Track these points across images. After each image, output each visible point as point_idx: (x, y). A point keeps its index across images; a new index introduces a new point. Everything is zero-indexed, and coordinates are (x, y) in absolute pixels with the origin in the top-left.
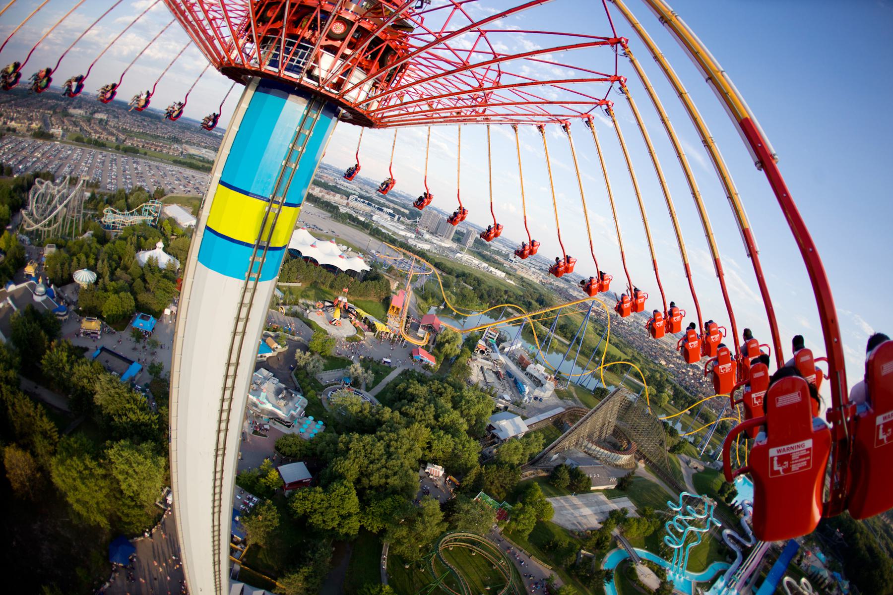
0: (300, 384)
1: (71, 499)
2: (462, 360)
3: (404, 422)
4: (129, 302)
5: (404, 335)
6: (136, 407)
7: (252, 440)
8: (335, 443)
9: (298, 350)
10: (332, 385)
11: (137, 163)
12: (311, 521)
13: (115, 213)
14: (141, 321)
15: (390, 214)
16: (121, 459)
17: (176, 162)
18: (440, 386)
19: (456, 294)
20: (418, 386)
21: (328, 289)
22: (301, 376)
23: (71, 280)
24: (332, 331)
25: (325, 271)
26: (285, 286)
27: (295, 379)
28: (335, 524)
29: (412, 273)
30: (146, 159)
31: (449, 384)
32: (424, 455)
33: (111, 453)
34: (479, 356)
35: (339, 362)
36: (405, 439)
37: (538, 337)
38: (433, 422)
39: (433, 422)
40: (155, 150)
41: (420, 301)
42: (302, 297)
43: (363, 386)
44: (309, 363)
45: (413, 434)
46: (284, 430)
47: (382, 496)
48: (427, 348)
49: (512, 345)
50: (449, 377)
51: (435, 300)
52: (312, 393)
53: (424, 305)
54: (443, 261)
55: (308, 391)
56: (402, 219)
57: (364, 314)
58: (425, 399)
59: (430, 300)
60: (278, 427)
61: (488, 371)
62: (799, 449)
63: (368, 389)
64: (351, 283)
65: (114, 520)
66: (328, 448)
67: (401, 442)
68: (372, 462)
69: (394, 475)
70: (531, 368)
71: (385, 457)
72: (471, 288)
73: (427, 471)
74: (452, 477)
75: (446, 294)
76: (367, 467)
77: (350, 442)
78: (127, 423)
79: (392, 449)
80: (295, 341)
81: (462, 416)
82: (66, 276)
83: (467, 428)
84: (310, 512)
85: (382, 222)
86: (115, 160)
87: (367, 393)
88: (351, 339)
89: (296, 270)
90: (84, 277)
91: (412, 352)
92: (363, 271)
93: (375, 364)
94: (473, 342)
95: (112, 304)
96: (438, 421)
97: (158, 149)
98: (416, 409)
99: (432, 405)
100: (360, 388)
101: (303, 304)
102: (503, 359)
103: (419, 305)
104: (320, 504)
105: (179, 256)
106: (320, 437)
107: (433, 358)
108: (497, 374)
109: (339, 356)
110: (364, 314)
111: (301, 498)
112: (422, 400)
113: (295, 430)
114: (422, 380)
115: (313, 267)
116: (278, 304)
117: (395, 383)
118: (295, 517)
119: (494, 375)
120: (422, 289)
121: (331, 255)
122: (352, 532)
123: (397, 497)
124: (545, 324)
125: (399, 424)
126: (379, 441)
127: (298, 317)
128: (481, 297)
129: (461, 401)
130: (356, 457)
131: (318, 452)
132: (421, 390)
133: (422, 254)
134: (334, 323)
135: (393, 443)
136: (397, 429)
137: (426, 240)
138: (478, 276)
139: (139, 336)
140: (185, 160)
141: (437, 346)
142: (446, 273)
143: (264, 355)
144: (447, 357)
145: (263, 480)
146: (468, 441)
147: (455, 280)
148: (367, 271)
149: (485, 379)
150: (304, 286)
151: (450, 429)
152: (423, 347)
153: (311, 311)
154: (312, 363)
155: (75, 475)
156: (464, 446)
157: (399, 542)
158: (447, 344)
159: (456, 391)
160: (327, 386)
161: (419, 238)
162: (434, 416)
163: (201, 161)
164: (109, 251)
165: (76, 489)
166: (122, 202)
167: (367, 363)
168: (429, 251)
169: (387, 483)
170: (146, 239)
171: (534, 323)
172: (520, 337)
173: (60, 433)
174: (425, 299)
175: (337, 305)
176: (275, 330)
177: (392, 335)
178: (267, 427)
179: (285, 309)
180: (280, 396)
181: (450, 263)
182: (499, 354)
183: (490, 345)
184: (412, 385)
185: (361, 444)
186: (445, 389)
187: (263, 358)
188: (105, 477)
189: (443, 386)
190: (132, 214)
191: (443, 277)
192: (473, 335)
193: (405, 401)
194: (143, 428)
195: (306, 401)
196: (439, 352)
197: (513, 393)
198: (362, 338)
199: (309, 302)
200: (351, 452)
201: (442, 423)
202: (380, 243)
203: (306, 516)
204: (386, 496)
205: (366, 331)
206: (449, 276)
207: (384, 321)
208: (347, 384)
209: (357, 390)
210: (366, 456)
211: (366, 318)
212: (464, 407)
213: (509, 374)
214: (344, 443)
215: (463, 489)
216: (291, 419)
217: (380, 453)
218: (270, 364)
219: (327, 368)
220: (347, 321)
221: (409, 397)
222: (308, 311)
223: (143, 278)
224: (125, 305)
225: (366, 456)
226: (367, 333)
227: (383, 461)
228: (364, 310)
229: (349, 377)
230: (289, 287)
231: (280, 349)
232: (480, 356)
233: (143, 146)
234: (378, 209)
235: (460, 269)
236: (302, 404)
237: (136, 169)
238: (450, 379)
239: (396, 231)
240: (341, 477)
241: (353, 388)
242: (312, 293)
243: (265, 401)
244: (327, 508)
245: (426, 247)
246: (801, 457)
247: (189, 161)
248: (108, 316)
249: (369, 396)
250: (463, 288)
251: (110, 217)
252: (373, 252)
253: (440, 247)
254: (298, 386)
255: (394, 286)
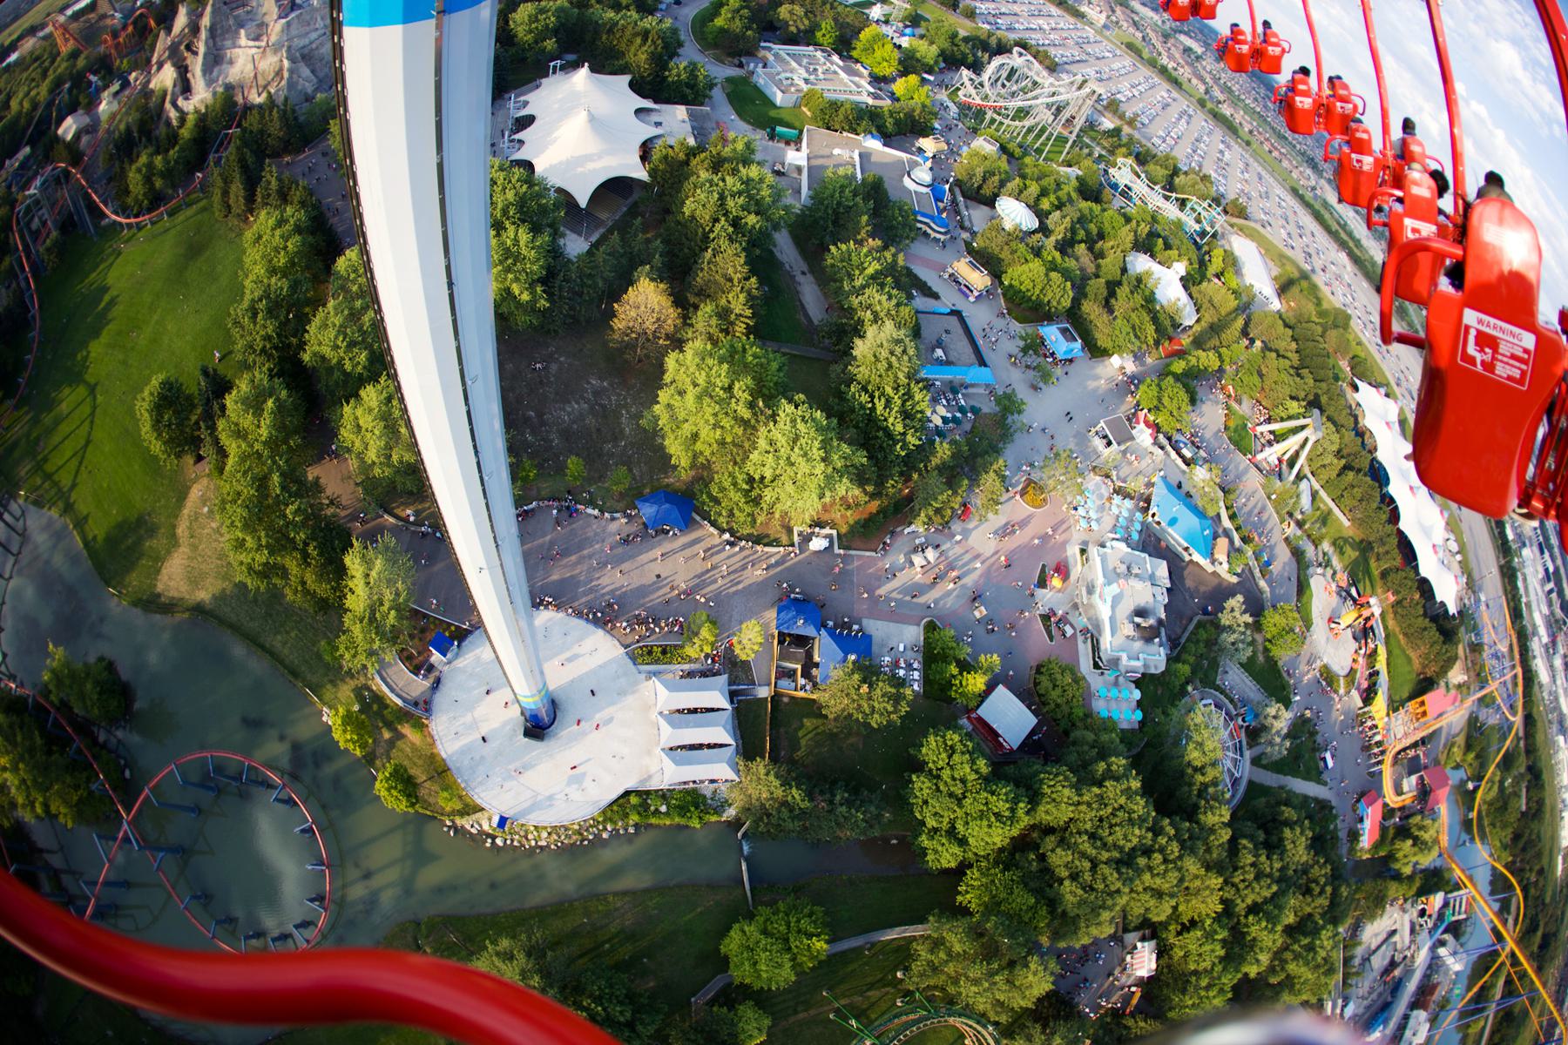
0: (1188, 640)
1: (663, 396)
2: (1394, 889)
3: (1215, 855)
4: (1059, 295)
5: (1388, 758)
6: (899, 402)
7: (1029, 621)
8: (1103, 755)
9: (1240, 598)
10: (1226, 696)
11: (1228, 147)
12: (914, 778)
13: (1139, 177)
14: (1058, 332)
15: (1546, 570)
16: (788, 427)
17: (1295, 192)
18: (1323, 881)
19: (1502, 788)
20: (1302, 842)
21: (1376, 573)
22: (1203, 635)
23: (990, 202)
24: (1319, 630)
25: (1394, 541)
26: (1326, 504)
27: (1191, 627)
28: (931, 823)
29: (1493, 686)
30: (1247, 151)
31: (1335, 893)
32: (1164, 925)
33: (786, 409)
34: (1413, 913)
35: (1274, 681)
36: (1176, 874)
37: (1482, 988)
38: (1241, 907)
39: (1241, 907)
40: (1270, 152)
41: (1461, 740)
42: (1334, 544)
43: (1257, 750)
44: (1234, 632)
45: (1198, 883)
46: (1085, 665)
47: (1032, 885)
48: (1388, 812)
49: (1454, 953)
50: (1349, 885)
51: (1476, 764)
52: (1184, 669)
53: (1457, 753)
54: (1539, 724)
55: (1184, 662)
56: (1554, 595)
57: (1381, 664)
58: (1281, 870)
59: (1471, 756)
60: (1084, 649)
61: (1391, 948)
62: (1511, 339)
63: (1256, 761)
64: (1412, 599)
65: (703, 473)
66: (1086, 748)
67: (1166, 871)
68: (1093, 836)
69: (1083, 889)
70: (1421, 1015)
71: (1116, 854)
72: (1524, 808)
73: (1139, 945)
74: (1138, 995)
75: (1494, 774)
76: (1079, 833)
77: (1117, 779)
78: (862, 407)
79: (1142, 861)
80: (1257, 585)
81: (1278, 955)
82: (987, 191)
83: (1252, 975)
84: (931, 770)
85: (1529, 570)
86: (1190, 116)
87: (1248, 763)
88: (1328, 676)
89: (1359, 496)
90: (1014, 213)
91: (1369, 790)
92: (1443, 604)
93: (1310, 744)
94: (1436, 884)
95: (1026, 274)
96: (1246, 917)
97: (1275, 154)
98: (1253, 865)
99: (1275, 888)
100: (1250, 746)
101: (1325, 554)
102: (1422, 957)
103: (1453, 744)
104: (954, 779)
105: (1202, 311)
106: (1108, 725)
107: (1377, 836)
108: (1393, 964)
109: (1285, 675)
110: (1381, 664)
111: (949, 743)
112: (1277, 865)
113: (1095, 681)
114: (1321, 843)
115: (1384, 517)
116: (1290, 515)
117: (1289, 799)
118: (912, 751)
119: (1386, 962)
120: (1480, 728)
121: (1426, 532)
122: (930, 857)
123: (1044, 911)
124: (1509, 982)
125: (1208, 850)
126: (1148, 829)
127: (1298, 562)
128: (1517, 837)
129: (1305, 935)
130: (1089, 804)
131: (1072, 735)
132: (1298, 848)
133: (1529, 677)
134: (1333, 625)
135: (1158, 857)
136: (1193, 851)
137: (1552, 666)
138: (1547, 802)
139: (1035, 346)
140: (1312, 202)
141: (1400, 826)
142: (1526, 745)
143: (1191, 550)
144: (1391, 857)
145: (954, 670)
146: (1222, 991)
147: (1522, 770)
148: (1446, 611)
149: (1375, 951)
150: (1351, 533)
151: (1238, 946)
152: (1385, 805)
153: (1324, 575)
154: (1235, 636)
155: (701, 380)
156: (1208, 988)
157: (937, 944)
158: (1410, 842)
159: (1323, 916)
160: (1217, 688)
161: (1547, 651)
162: (1255, 904)
163: (1339, 224)
164: (1087, 212)
165: (682, 393)
166: (1161, 173)
167: (1303, 730)
168: (1541, 686)
169: (1061, 881)
170: (1168, 247)
171: (1503, 964)
172: (1474, 957)
173: (749, 330)
174: (1468, 747)
175: (1362, 606)
176: (1245, 540)
177: (1378, 738)
178: (1069, 631)
179: (1291, 530)
180: (1137, 620)
181: (1543, 738)
182: (1429, 944)
183: (1441, 916)
184: (1298, 830)
185: (1122, 800)
186: (1320, 894)
187: (1185, 554)
188: (745, 423)
189: (1325, 885)
190: (1167, 198)
191: (1517, 745)
192: (1446, 875)
193: (1261, 836)
194: (881, 434)
195: (1162, 668)
196: (1393, 839)
197: (1364, 1014)
198: (1342, 691)
199: (1335, 561)
200: (1096, 790)
201: (1247, 925)
202: (1501, 592)
203: (919, 767)
204: (1038, 892)
205: (1358, 689)
206: (1523, 754)
207: (1394, 706)
208: (1243, 720)
209: (1244, 743)
210: (1101, 820)
211: (1377, 673)
212: (1296, 947)
213: (1397, 987)
214: (1109, 769)
215: (1119, 1024)
216: (1109, 661)
217: (1122, 843)
218: (1186, 573)
219: (1248, 666)
220: (1354, 645)
221: (1274, 839)
222: (1320, 570)
223: (1112, 287)
224: (1050, 295)
225: (1101, 820)
226: (1354, 693)
227: (1105, 855)
228: (1388, 659)
229: (1256, 716)
230: (1330, 512)
231: (1223, 570)
232: (1415, 914)
233: (1251, 132)
234: (1540, 545)
235: (1543, 763)
236: (1152, 664)
237: (1221, 152)
238: (1344, 891)
239: (1534, 606)
240: (1034, 798)
241: (1243, 735)
242: (1352, 554)
243: (1109, 600)
244: (951, 795)
245: (1543, 676)
246: (1513, 357)
247: (1317, 206)
248: (1011, 286)
249: (1246, 771)
250: (1517, 795)
251: (1123, 173)
252: (1483, 598)
253: (1556, 699)
254: (1183, 640)
255: (1457, 675)
